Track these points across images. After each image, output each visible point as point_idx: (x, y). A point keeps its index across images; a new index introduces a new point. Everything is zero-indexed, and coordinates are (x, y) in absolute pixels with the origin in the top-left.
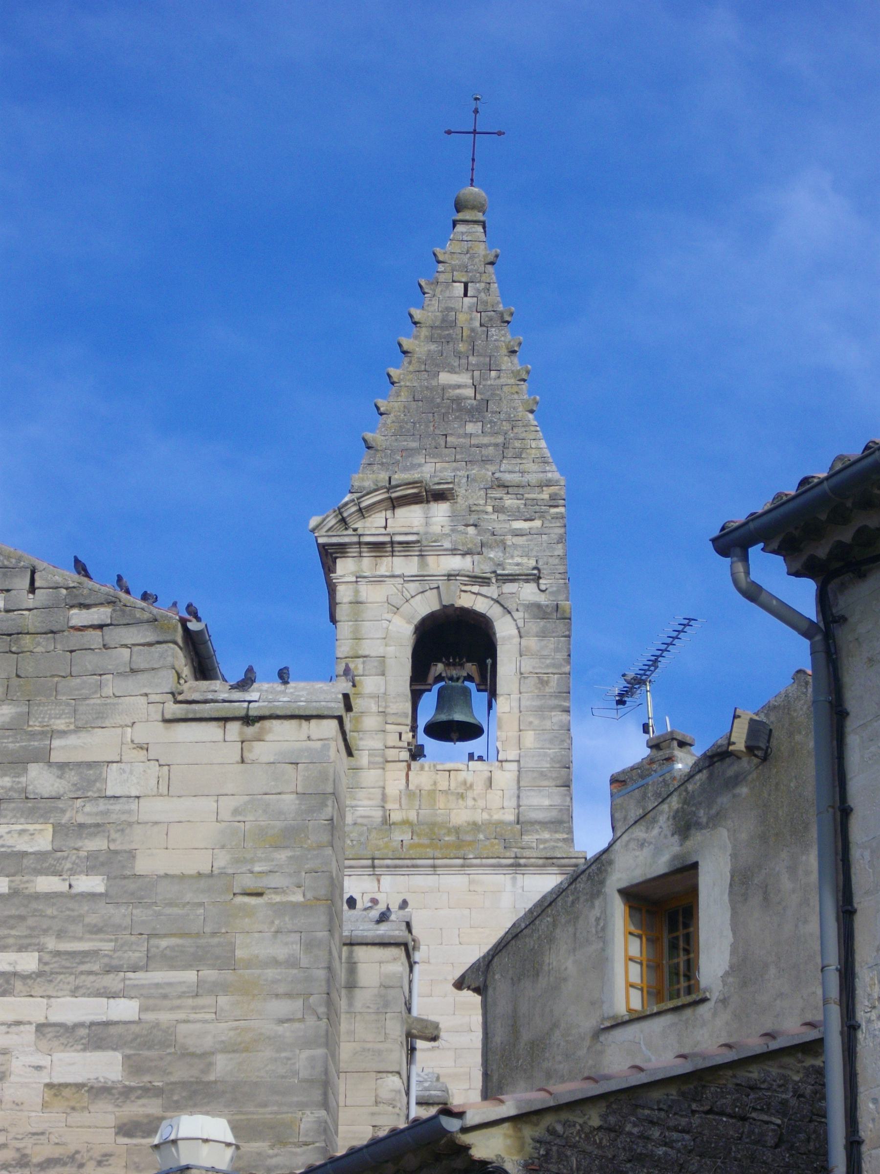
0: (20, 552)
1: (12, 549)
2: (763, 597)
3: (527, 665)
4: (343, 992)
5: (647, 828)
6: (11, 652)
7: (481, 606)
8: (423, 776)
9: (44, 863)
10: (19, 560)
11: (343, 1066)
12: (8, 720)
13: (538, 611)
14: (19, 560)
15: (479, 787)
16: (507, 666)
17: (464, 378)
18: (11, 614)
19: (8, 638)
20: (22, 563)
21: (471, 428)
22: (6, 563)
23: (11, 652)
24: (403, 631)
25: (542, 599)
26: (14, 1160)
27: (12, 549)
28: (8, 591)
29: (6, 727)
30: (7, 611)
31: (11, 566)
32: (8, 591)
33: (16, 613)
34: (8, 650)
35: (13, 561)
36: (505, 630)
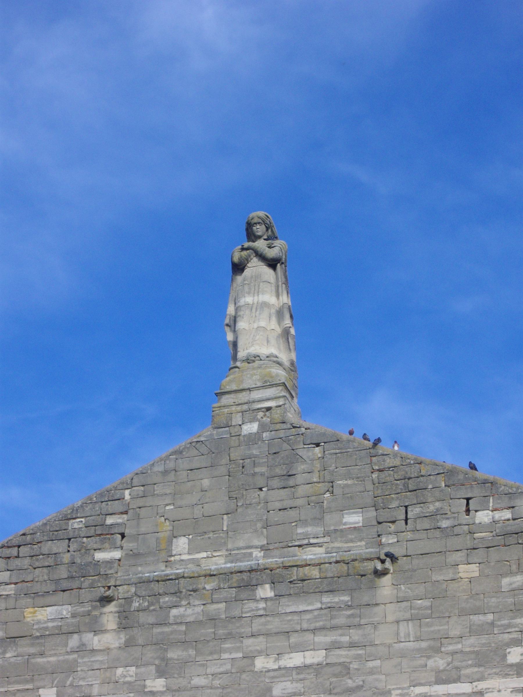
0: (518, 484)
1: (513, 483)
2: (235, 340)
4: (273, 572)
5: (241, 257)
6: (519, 543)
9: (33, 655)
10: (518, 488)
11: (299, 569)
12: (521, 584)
14: (518, 488)
18: (517, 521)
19: (516, 535)
20: (520, 490)
22: (510, 491)
23: (519, 543)
26: (509, 653)
27: (513, 483)
28: (513, 507)
29: (521, 588)
30: (514, 519)
31: (513, 492)
32: (513, 507)
33: (519, 520)
34: (516, 542)
35: (515, 489)
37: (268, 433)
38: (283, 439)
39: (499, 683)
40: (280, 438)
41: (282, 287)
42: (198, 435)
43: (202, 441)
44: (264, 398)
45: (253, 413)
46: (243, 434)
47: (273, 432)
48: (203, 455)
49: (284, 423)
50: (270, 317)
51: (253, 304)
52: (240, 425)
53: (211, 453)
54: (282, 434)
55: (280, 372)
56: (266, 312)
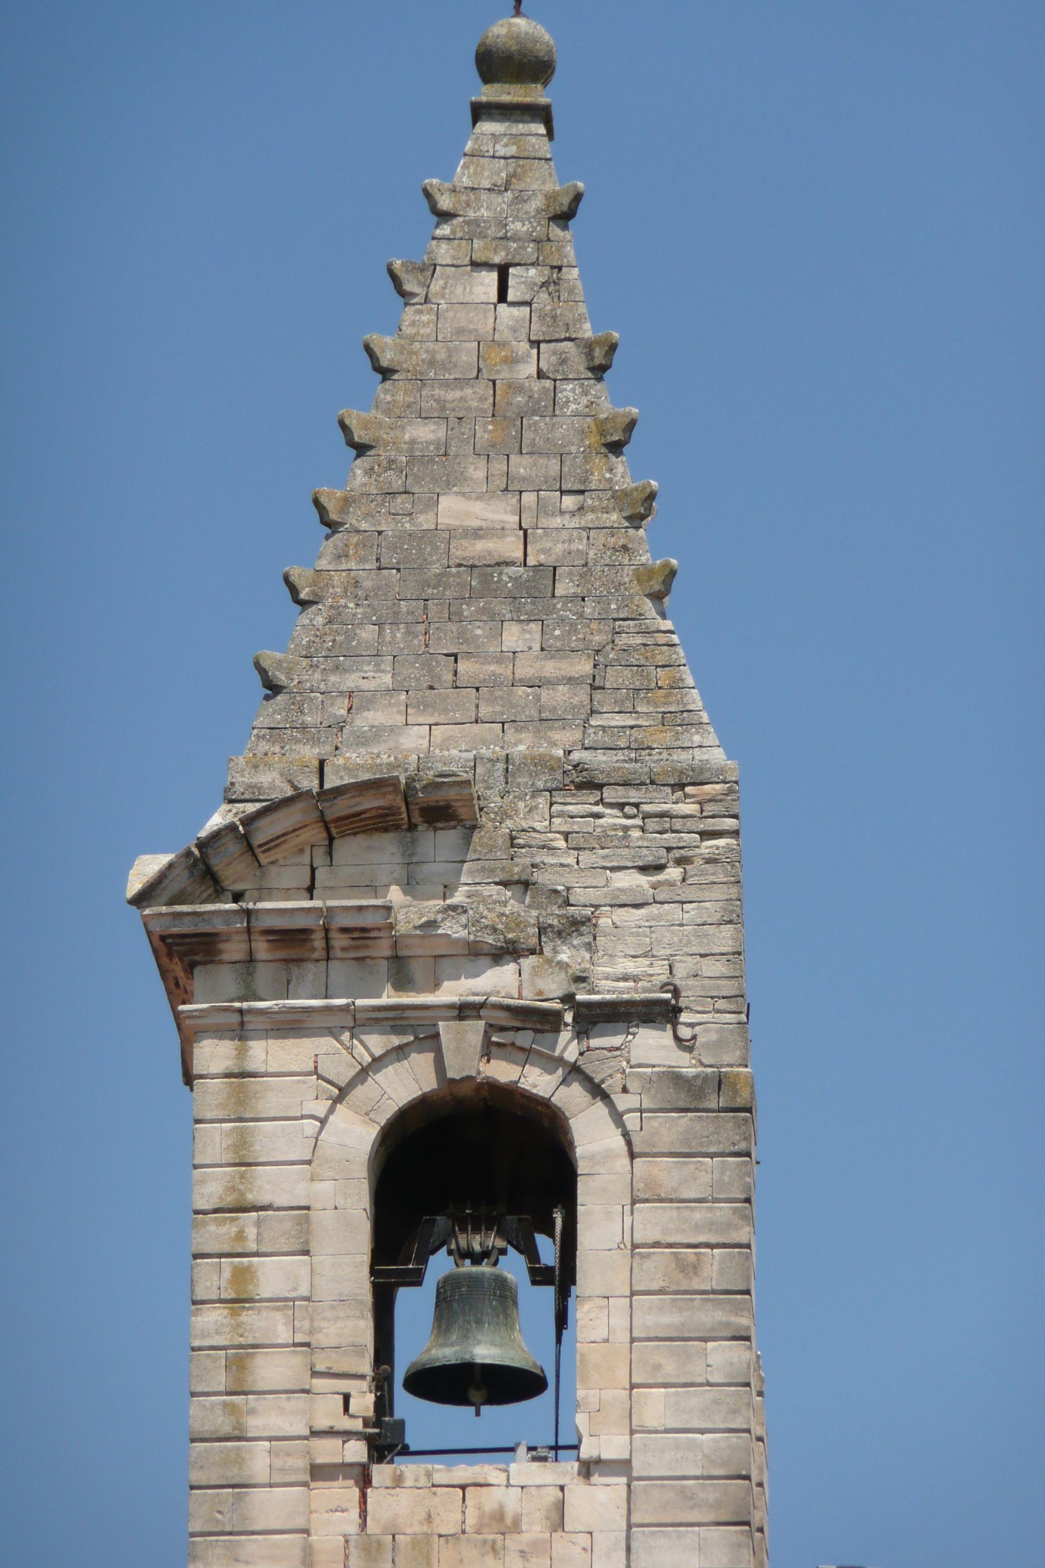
3: (652, 1222)
7: (538, 1081)
8: (403, 1495)
13: (688, 1093)
15: (534, 1529)
16: (602, 1221)
17: (500, 513)
21: (513, 637)
24: (356, 1135)
25: (686, 1065)
36: (593, 1136)
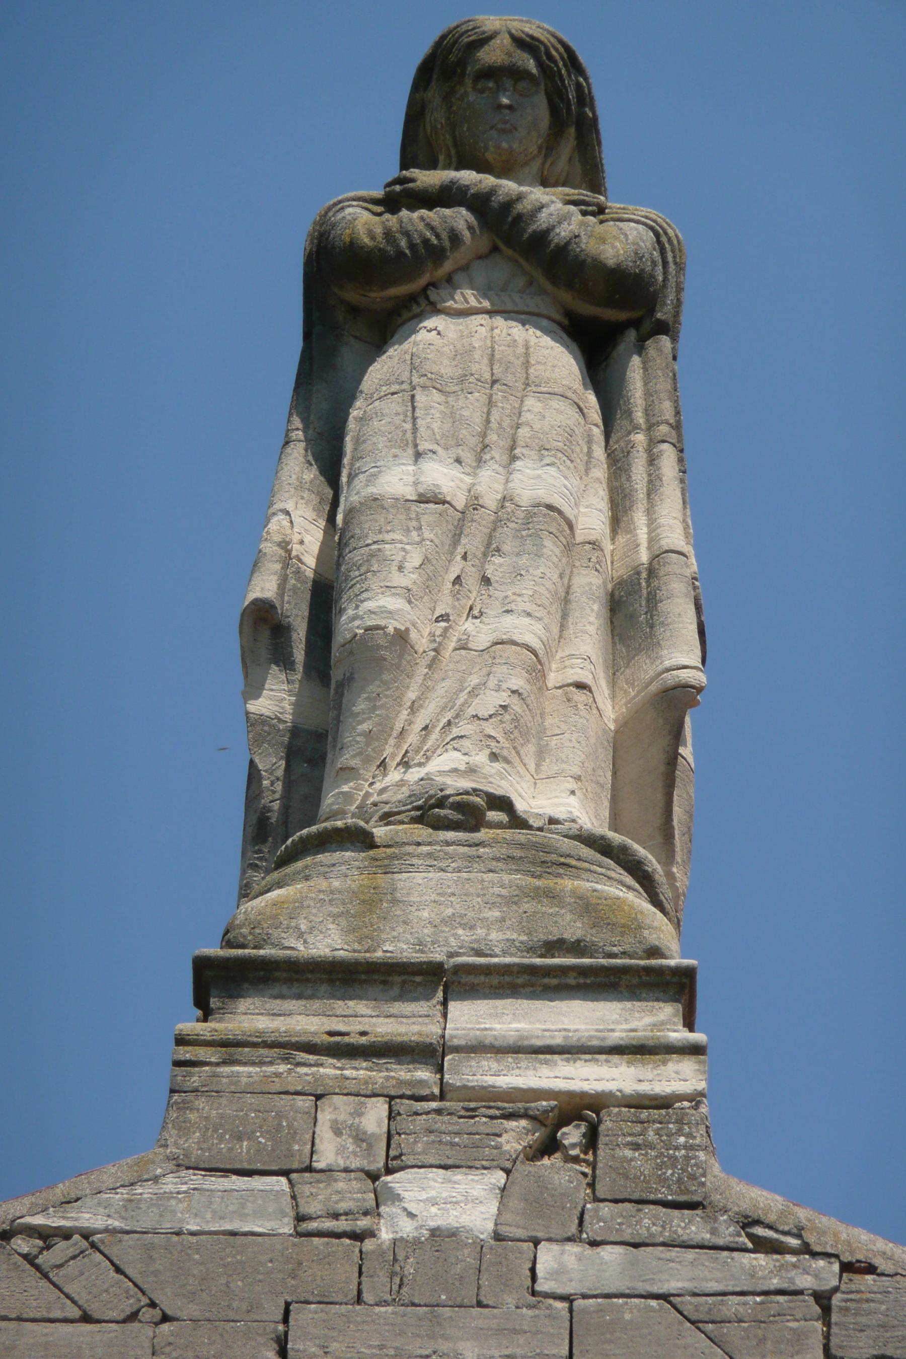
37: (573, 1249)
38: (688, 1303)
39: (305, 918)
40: (664, 1297)
41: (652, 460)
42: (60, 1190)
43: (86, 1235)
44: (558, 1040)
45: (471, 1113)
46: (385, 1235)
47: (609, 1253)
48: (86, 1318)
49: (692, 1206)
50: (565, 616)
51: (475, 503)
52: (374, 1177)
53: (148, 1314)
54: (678, 1274)
55: (630, 896)
56: (544, 570)
